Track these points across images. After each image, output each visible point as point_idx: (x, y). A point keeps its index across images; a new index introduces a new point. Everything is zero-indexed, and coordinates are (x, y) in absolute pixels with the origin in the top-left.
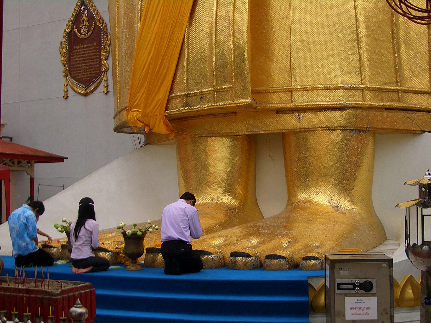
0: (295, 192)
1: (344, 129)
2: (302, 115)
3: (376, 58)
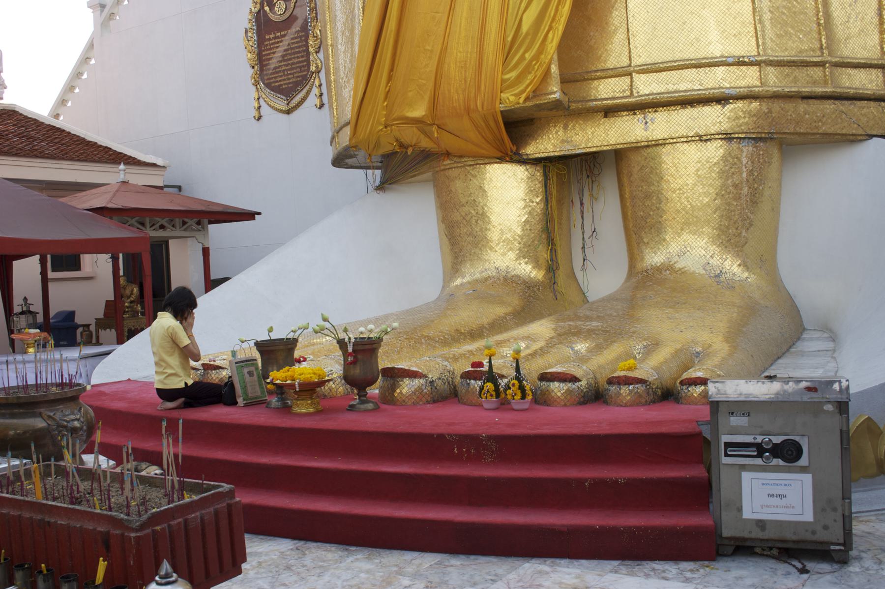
0: (642, 252)
1: (728, 137)
2: (650, 116)
3: (784, 7)
